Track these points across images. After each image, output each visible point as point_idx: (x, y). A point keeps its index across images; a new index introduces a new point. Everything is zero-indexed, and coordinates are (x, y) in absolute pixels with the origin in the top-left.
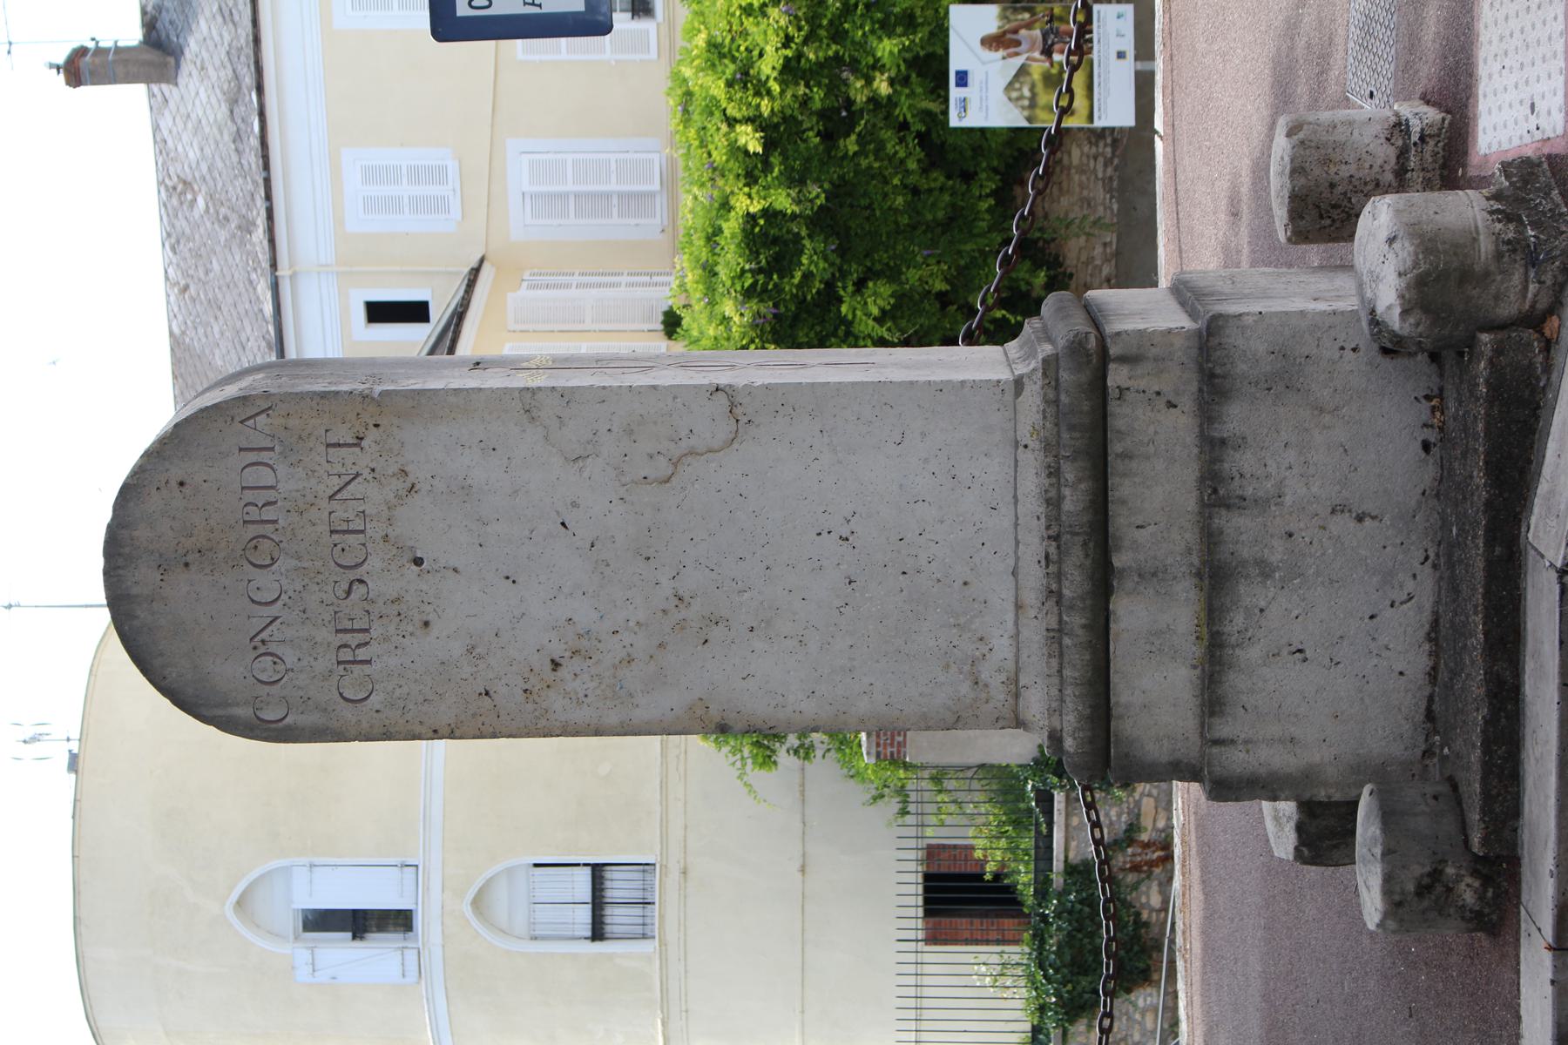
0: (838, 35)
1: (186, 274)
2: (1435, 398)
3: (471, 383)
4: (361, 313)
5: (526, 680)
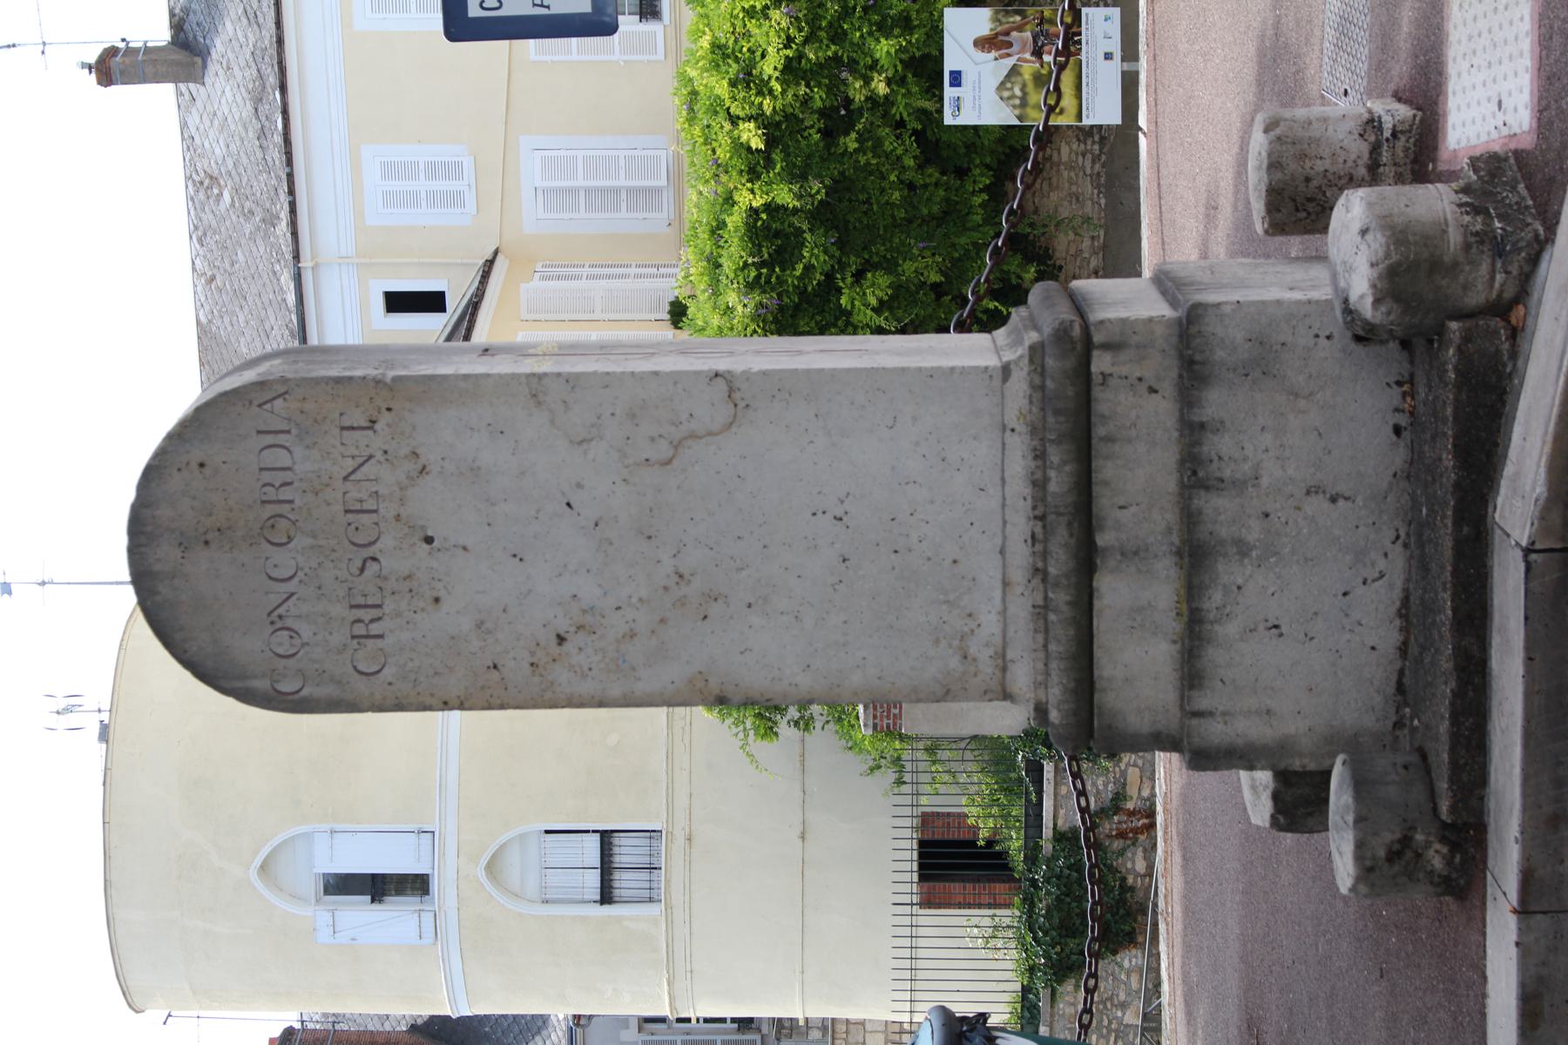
0: (837, 36)
1: (212, 265)
2: (1407, 384)
4: (380, 303)
5: (533, 654)
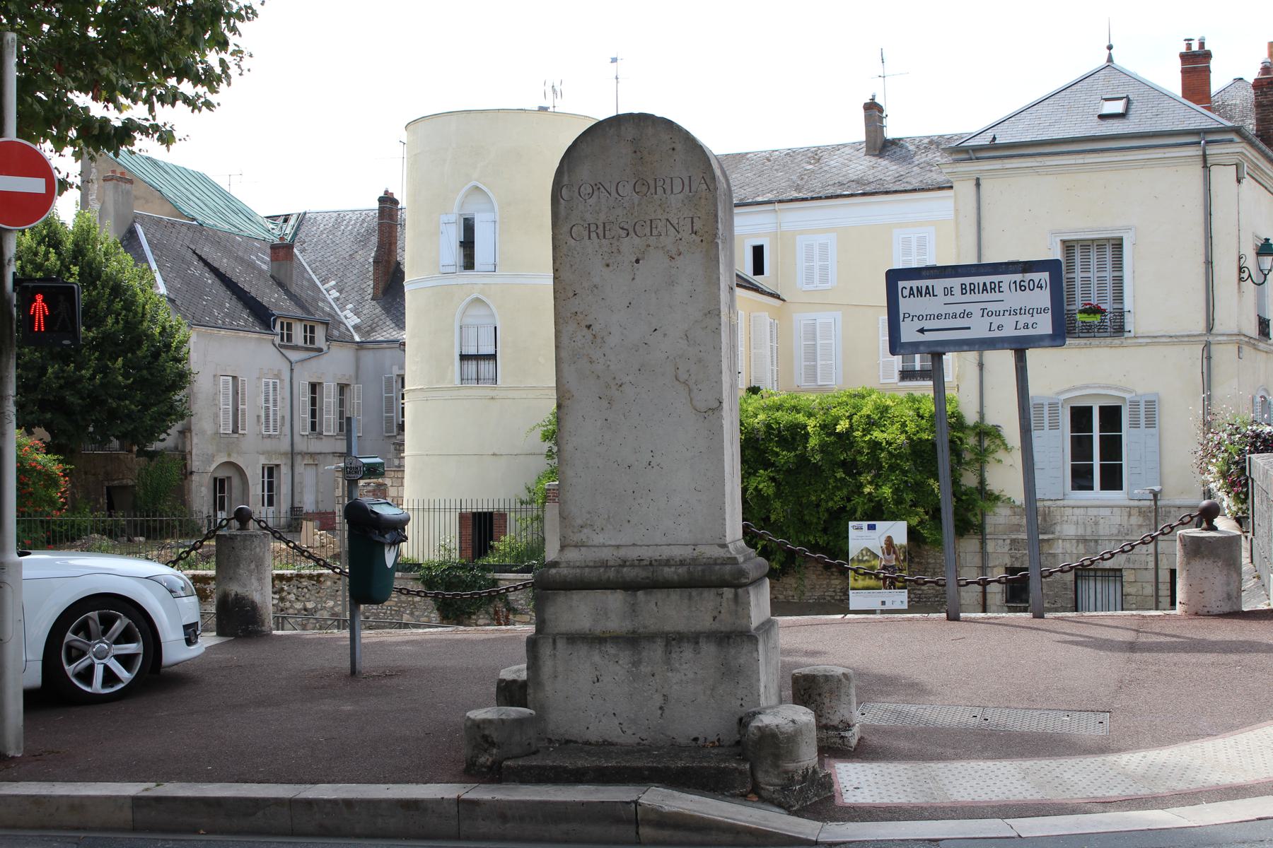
0: (892, 468)
1: (776, 160)
2: (719, 744)
3: (722, 285)
4: (758, 243)
